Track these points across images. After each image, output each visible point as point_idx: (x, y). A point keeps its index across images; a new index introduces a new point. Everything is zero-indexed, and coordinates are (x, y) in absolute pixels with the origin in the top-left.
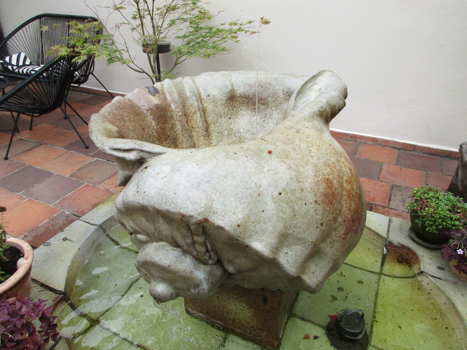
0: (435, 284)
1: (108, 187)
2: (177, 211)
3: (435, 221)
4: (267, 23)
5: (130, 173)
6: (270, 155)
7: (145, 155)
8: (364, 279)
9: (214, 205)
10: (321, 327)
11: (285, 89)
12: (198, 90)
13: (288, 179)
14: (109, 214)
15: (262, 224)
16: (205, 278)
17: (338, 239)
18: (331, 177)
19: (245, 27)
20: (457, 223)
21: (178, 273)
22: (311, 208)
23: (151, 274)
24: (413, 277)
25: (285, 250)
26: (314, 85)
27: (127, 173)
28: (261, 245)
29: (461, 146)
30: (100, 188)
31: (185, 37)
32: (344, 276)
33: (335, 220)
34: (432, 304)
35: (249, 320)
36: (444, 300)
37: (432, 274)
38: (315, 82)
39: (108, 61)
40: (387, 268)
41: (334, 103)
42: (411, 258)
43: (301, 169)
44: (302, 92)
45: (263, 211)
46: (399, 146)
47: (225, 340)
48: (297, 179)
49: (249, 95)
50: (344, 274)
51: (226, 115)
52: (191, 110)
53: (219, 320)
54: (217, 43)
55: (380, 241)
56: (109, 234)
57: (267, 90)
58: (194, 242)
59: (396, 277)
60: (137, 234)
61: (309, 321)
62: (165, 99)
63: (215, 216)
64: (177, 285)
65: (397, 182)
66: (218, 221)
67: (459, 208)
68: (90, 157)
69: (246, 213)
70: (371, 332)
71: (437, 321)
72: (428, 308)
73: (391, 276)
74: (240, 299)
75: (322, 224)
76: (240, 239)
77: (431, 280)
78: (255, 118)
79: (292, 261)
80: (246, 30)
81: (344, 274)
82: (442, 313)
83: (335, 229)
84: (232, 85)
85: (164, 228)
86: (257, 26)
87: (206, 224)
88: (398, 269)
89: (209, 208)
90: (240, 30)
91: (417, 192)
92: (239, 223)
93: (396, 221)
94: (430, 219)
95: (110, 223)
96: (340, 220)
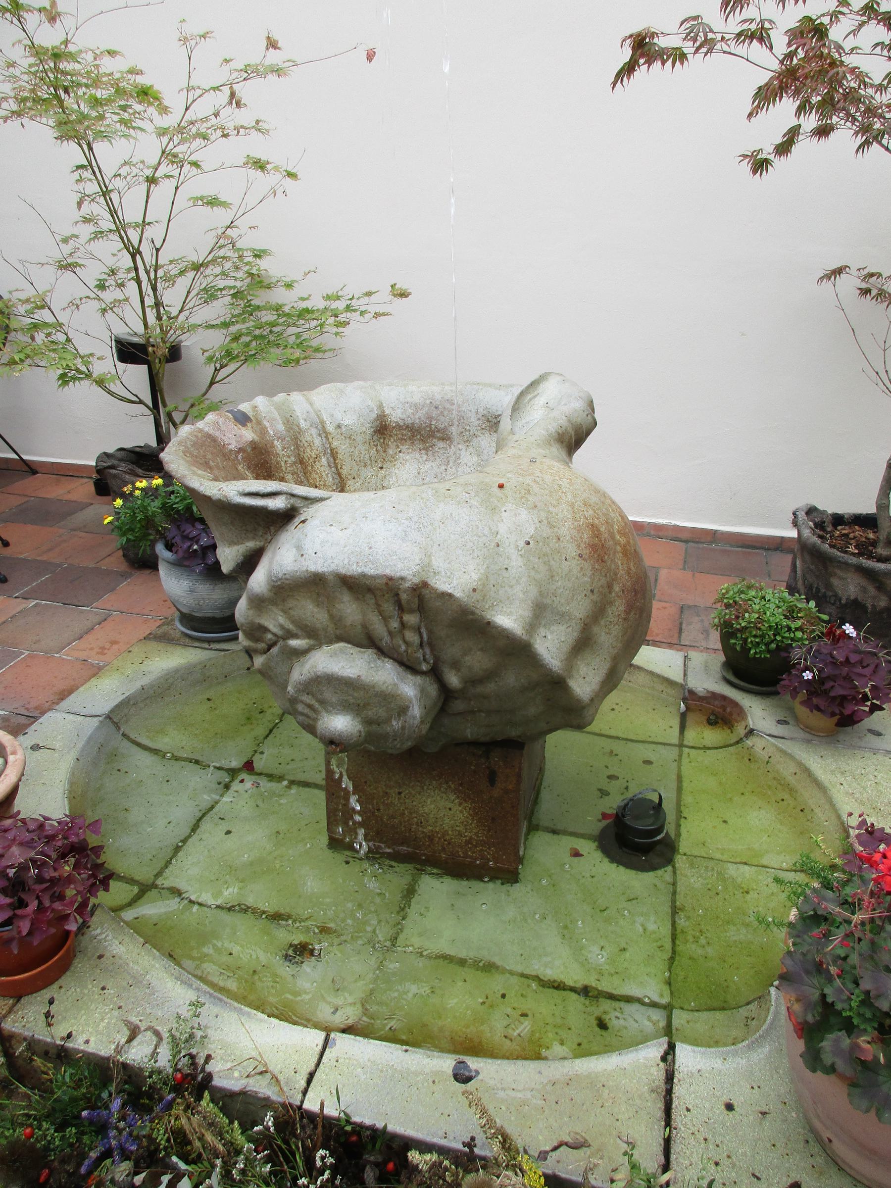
0: (776, 746)
1: (82, 655)
2: (380, 571)
3: (762, 636)
4: (403, 295)
5: (258, 543)
6: (503, 491)
7: (298, 503)
8: (652, 757)
9: (434, 562)
10: (589, 839)
11: (481, 410)
12: (318, 417)
13: (537, 521)
14: (119, 693)
15: (507, 588)
16: (415, 695)
17: (616, 619)
18: (596, 521)
20: (799, 634)
21: (373, 687)
22: (574, 565)
23: (322, 702)
24: (738, 742)
25: (542, 631)
26: (535, 397)
27: (251, 544)
28: (508, 619)
29: (794, 514)
30: (63, 659)
31: (225, 325)
32: (616, 755)
33: (610, 586)
34: (774, 778)
37: (768, 733)
38: (536, 393)
39: (59, 379)
40: (691, 736)
42: (731, 714)
43: (552, 509)
44: (518, 409)
45: (507, 569)
46: (684, 536)
47: (410, 892)
48: (549, 523)
49: (413, 424)
50: (615, 753)
51: (373, 463)
52: (309, 453)
53: (402, 844)
54: (305, 336)
55: (673, 692)
56: (126, 732)
57: (446, 413)
58: (403, 625)
59: (709, 748)
60: (288, 638)
62: (263, 432)
63: (437, 577)
65: (690, 600)
66: (442, 584)
67: (800, 610)
68: (18, 600)
69: (482, 571)
70: (678, 835)
71: (785, 802)
72: (769, 787)
73: (699, 748)
74: (444, 786)
75: (592, 591)
76: (477, 611)
77: (768, 741)
78: (428, 465)
79: (554, 650)
80: (363, 309)
81: (615, 753)
82: (792, 790)
83: (611, 603)
84: (381, 406)
85: (350, 610)
86: (382, 300)
87: (425, 592)
88: (711, 736)
89: (426, 566)
90: (348, 308)
91: (727, 592)
93: (697, 658)
94: (754, 633)
95: (126, 711)
96: (617, 588)
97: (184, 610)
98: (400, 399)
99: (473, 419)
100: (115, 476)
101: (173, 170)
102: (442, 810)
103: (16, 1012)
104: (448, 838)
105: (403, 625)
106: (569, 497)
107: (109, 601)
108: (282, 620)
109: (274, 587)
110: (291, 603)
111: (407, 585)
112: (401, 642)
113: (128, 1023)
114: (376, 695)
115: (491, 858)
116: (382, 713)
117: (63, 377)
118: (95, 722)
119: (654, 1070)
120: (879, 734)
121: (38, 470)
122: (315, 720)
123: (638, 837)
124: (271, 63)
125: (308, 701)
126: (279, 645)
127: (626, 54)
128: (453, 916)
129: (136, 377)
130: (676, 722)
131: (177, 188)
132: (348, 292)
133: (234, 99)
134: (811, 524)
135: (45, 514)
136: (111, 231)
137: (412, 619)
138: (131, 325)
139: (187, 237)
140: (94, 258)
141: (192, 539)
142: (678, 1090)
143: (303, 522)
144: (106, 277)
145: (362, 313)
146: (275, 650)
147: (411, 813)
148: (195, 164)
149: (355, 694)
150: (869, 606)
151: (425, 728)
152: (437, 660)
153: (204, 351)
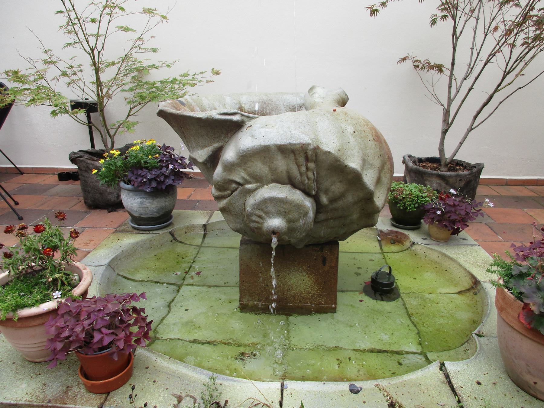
4: (217, 73)
7: (245, 119)
8: (372, 258)
11: (285, 103)
20: (427, 199)
21: (293, 202)
23: (267, 213)
24: (407, 249)
35: (309, 290)
36: (436, 255)
39: (51, 114)
42: (401, 238)
47: (287, 318)
57: (269, 106)
60: (245, 184)
61: (347, 291)
64: (291, 216)
66: (326, 147)
76: (341, 160)
84: (240, 103)
85: (282, 164)
87: (318, 151)
88: (394, 248)
92: (339, 148)
97: (136, 215)
100: (82, 161)
102: (301, 282)
103: (109, 400)
104: (302, 295)
105: (307, 169)
108: (243, 174)
109: (241, 156)
110: (249, 164)
111: (311, 147)
112: (306, 178)
113: (174, 395)
114: (295, 206)
115: (323, 303)
118: (103, 268)
119: (439, 374)
120: (465, 239)
121: (24, 172)
122: (261, 224)
123: (382, 288)
125: (259, 213)
126: (239, 190)
128: (310, 331)
130: (377, 244)
131: (109, 22)
132: (191, 73)
135: (34, 190)
136: (75, 43)
137: (311, 165)
139: (113, 49)
141: (142, 176)
142: (453, 381)
143: (250, 126)
144: (67, 69)
145: (199, 81)
147: (284, 285)
148: (122, 9)
149: (284, 206)
153: (126, 99)
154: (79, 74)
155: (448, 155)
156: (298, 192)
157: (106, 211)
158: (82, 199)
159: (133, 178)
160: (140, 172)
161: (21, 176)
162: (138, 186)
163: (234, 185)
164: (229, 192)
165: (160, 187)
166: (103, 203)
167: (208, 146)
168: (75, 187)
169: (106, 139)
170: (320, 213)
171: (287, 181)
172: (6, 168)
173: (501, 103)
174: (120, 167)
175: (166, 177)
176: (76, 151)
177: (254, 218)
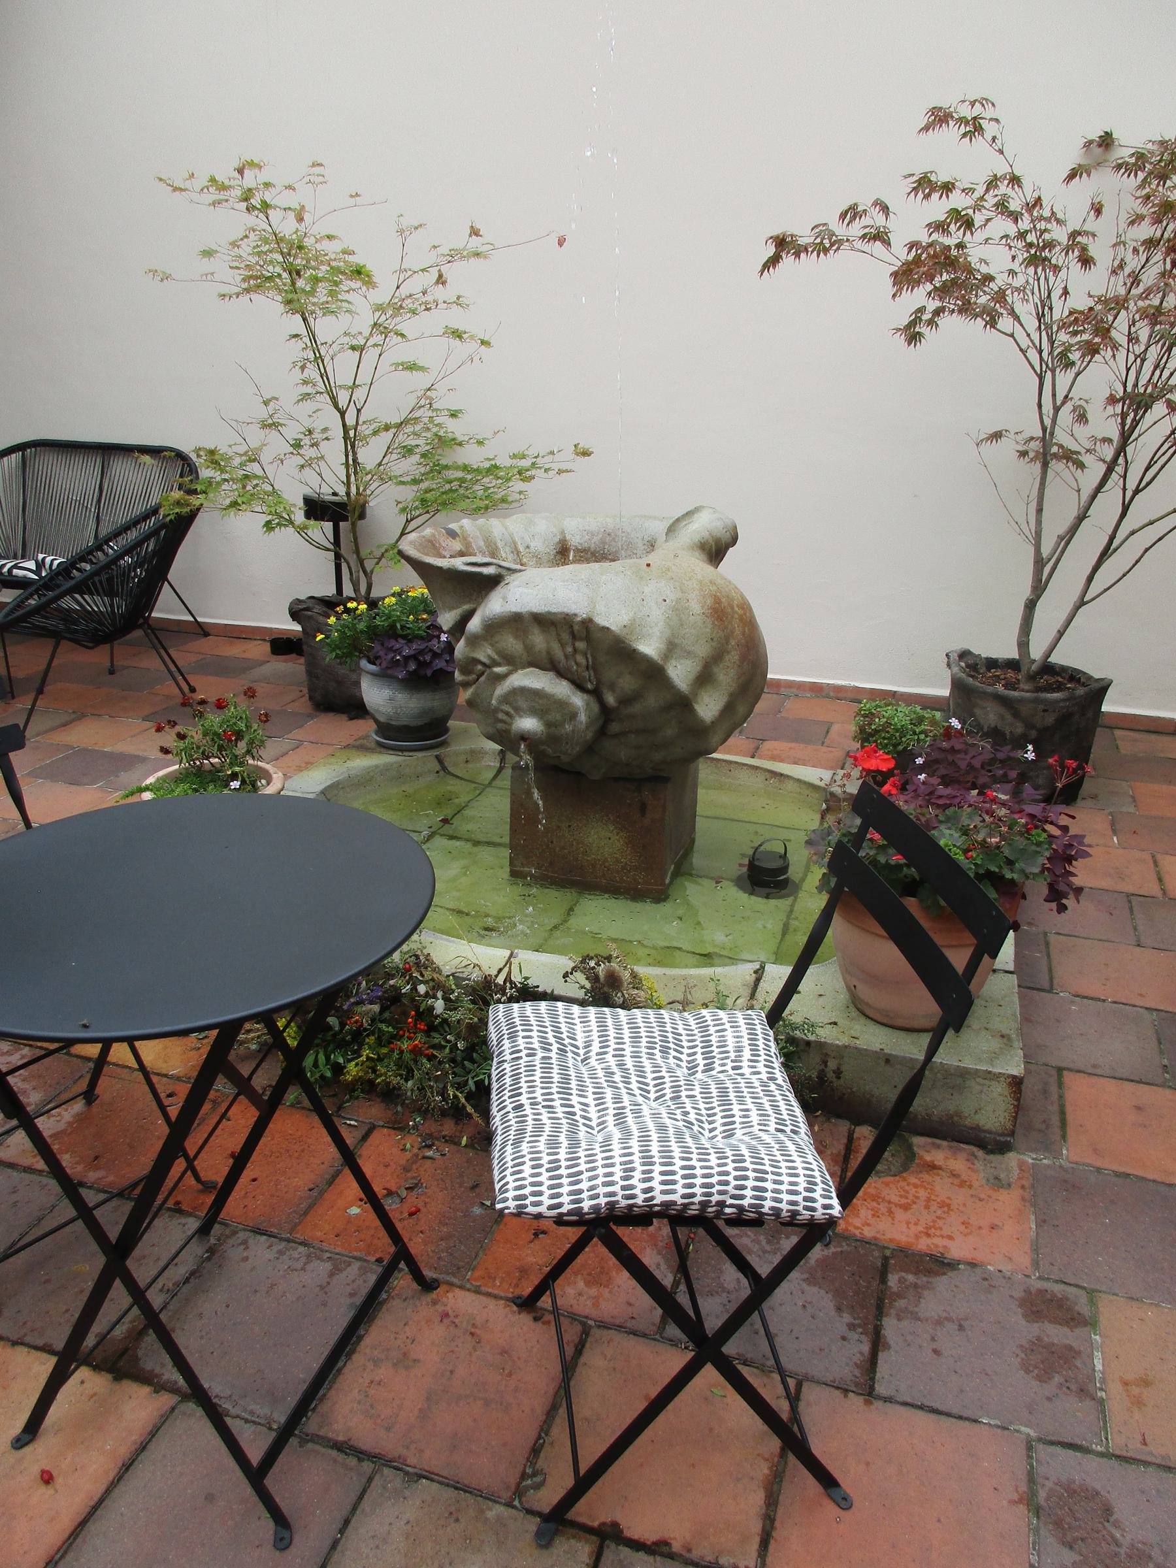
4: (586, 453)
7: (504, 572)
19: (543, 460)
23: (517, 709)
25: (673, 662)
27: (466, 607)
28: (649, 648)
31: (415, 482)
33: (727, 639)
41: (719, 535)
58: (575, 650)
66: (601, 621)
80: (547, 466)
84: (563, 532)
85: (539, 640)
96: (733, 642)
97: (382, 719)
98: (577, 531)
99: (640, 544)
100: (310, 617)
101: (378, 339)
102: (603, 840)
105: (575, 650)
106: (699, 577)
107: (297, 734)
108: (490, 651)
110: (498, 638)
116: (558, 717)
117: (268, 524)
119: (748, 977)
121: (211, 632)
122: (510, 724)
124: (474, 247)
127: (771, 250)
129: (322, 530)
130: (818, 816)
132: (532, 452)
133: (441, 280)
134: (963, 664)
135: (224, 668)
137: (581, 645)
138: (330, 482)
139: (388, 400)
140: (292, 418)
144: (302, 436)
145: (546, 471)
146: (483, 679)
150: (1007, 733)
151: (590, 735)
152: (599, 682)
153: (399, 503)
154: (323, 444)
155: (1036, 652)
156: (565, 683)
157: (344, 717)
158: (305, 690)
159: (381, 653)
160: (392, 643)
161: (204, 640)
162: (387, 668)
163: (480, 667)
164: (474, 676)
165: (422, 672)
166: (336, 701)
167: (457, 607)
168: (292, 667)
169: (358, 577)
170: (613, 721)
171: (548, 666)
172: (180, 621)
173: (1147, 550)
174: (362, 632)
175: (435, 655)
176: (303, 597)
177: (501, 716)
